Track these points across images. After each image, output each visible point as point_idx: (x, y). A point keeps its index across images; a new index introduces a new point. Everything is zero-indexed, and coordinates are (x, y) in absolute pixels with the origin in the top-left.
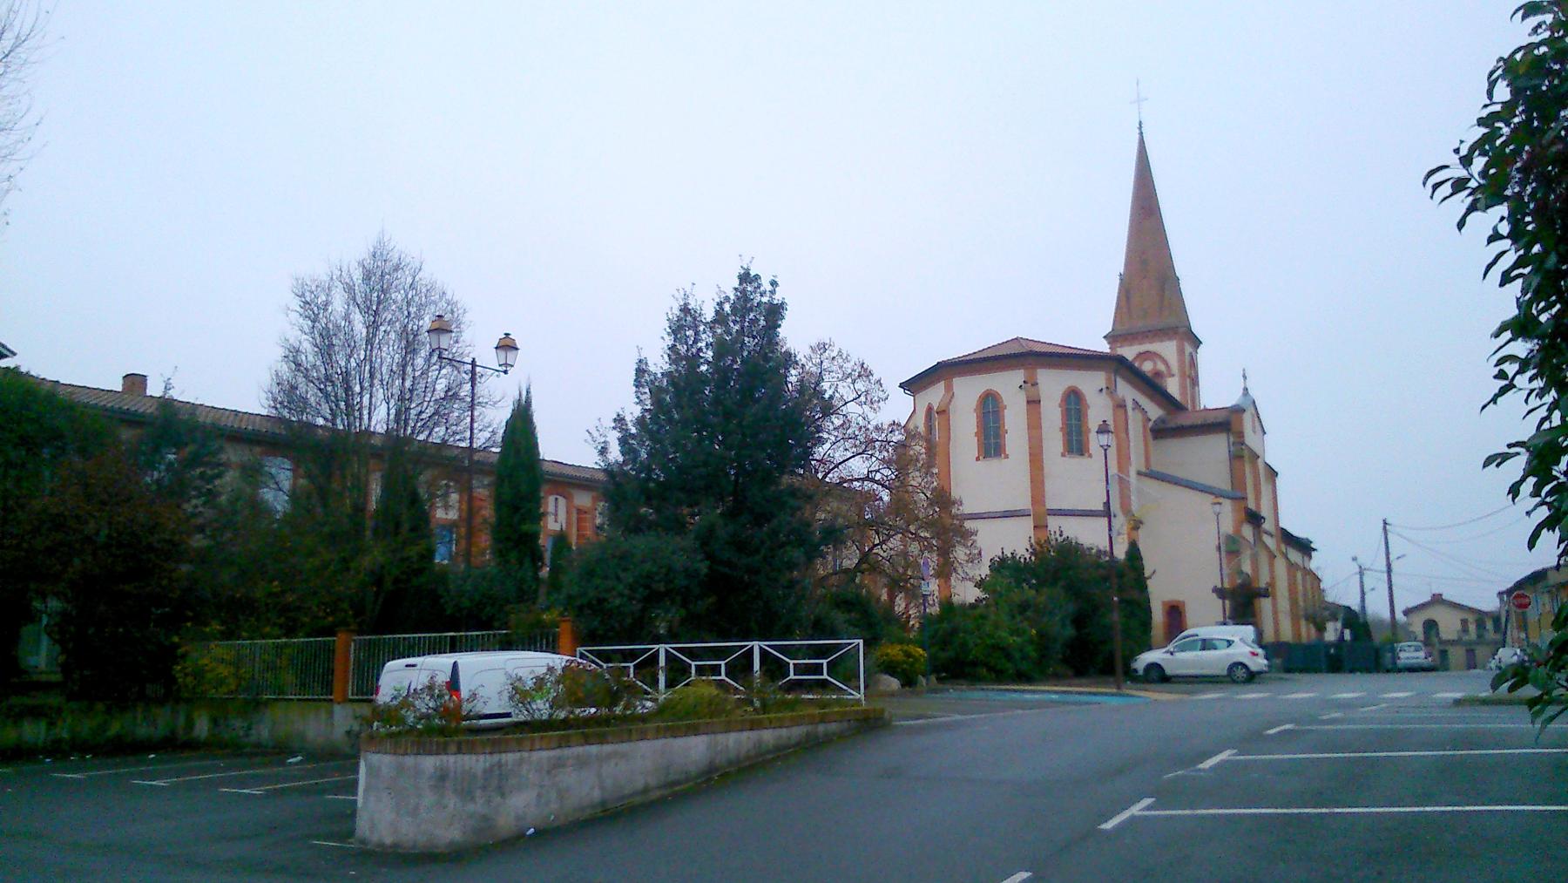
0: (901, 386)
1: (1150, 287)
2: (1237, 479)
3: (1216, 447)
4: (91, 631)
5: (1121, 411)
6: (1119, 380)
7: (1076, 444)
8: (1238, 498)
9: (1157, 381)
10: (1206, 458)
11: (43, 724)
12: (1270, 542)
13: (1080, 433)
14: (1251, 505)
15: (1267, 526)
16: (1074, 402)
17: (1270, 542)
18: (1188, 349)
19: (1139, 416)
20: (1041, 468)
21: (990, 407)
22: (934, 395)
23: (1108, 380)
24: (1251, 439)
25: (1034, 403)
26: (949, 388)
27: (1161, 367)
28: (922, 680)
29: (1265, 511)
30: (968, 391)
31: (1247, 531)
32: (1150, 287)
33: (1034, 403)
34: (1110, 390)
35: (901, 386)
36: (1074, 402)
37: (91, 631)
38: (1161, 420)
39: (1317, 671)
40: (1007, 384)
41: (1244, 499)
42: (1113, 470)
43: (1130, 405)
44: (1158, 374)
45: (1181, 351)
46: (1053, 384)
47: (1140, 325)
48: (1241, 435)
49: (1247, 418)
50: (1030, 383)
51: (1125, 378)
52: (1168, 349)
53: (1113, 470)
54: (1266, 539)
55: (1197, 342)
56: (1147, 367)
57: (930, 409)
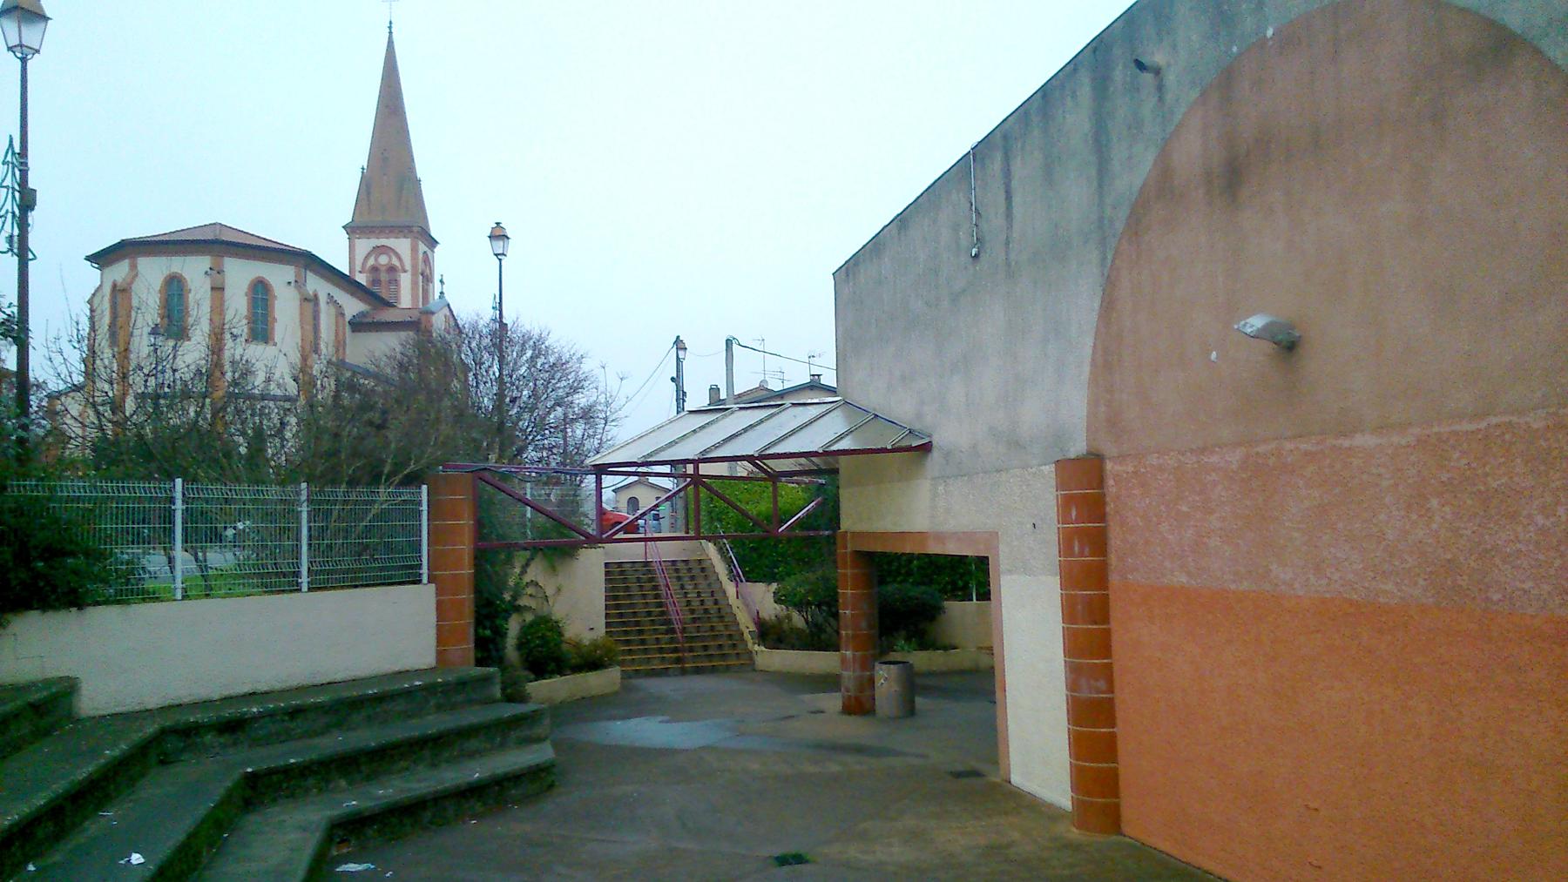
0: (88, 258)
1: (390, 195)
4: (1214, 355)
5: (309, 307)
6: (310, 275)
13: (265, 322)
16: (260, 293)
18: (422, 247)
19: (333, 310)
22: (120, 271)
25: (218, 289)
26: (133, 267)
27: (395, 262)
30: (153, 271)
32: (390, 195)
33: (218, 289)
34: (299, 284)
35: (88, 258)
36: (260, 293)
37: (1214, 355)
38: (362, 315)
39: (993, 718)
40: (194, 270)
43: (323, 299)
45: (414, 250)
46: (239, 274)
47: (377, 219)
52: (402, 245)
55: (433, 243)
57: (114, 286)
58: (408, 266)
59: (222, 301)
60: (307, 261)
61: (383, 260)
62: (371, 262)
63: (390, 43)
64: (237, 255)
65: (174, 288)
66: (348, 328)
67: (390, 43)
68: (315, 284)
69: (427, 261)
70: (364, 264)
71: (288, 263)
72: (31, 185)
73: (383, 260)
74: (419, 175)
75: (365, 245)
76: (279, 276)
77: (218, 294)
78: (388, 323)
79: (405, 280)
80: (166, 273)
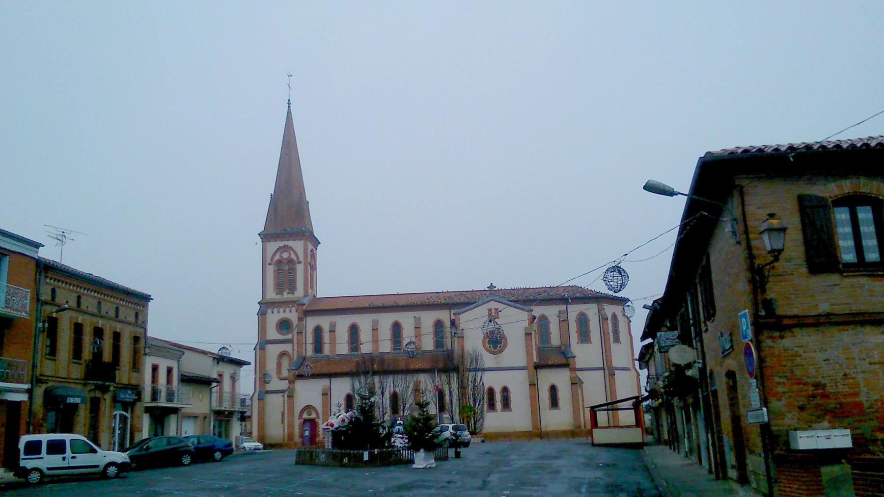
18: (310, 247)
27: (293, 256)
40: (551, 312)
45: (306, 250)
46: (574, 310)
52: (298, 246)
55: (316, 243)
58: (301, 259)
59: (293, 403)
61: (285, 255)
62: (277, 257)
63: (289, 112)
67: (289, 112)
69: (313, 256)
70: (272, 259)
73: (285, 255)
75: (273, 246)
78: (325, 310)
79: (300, 269)
80: (795, 197)
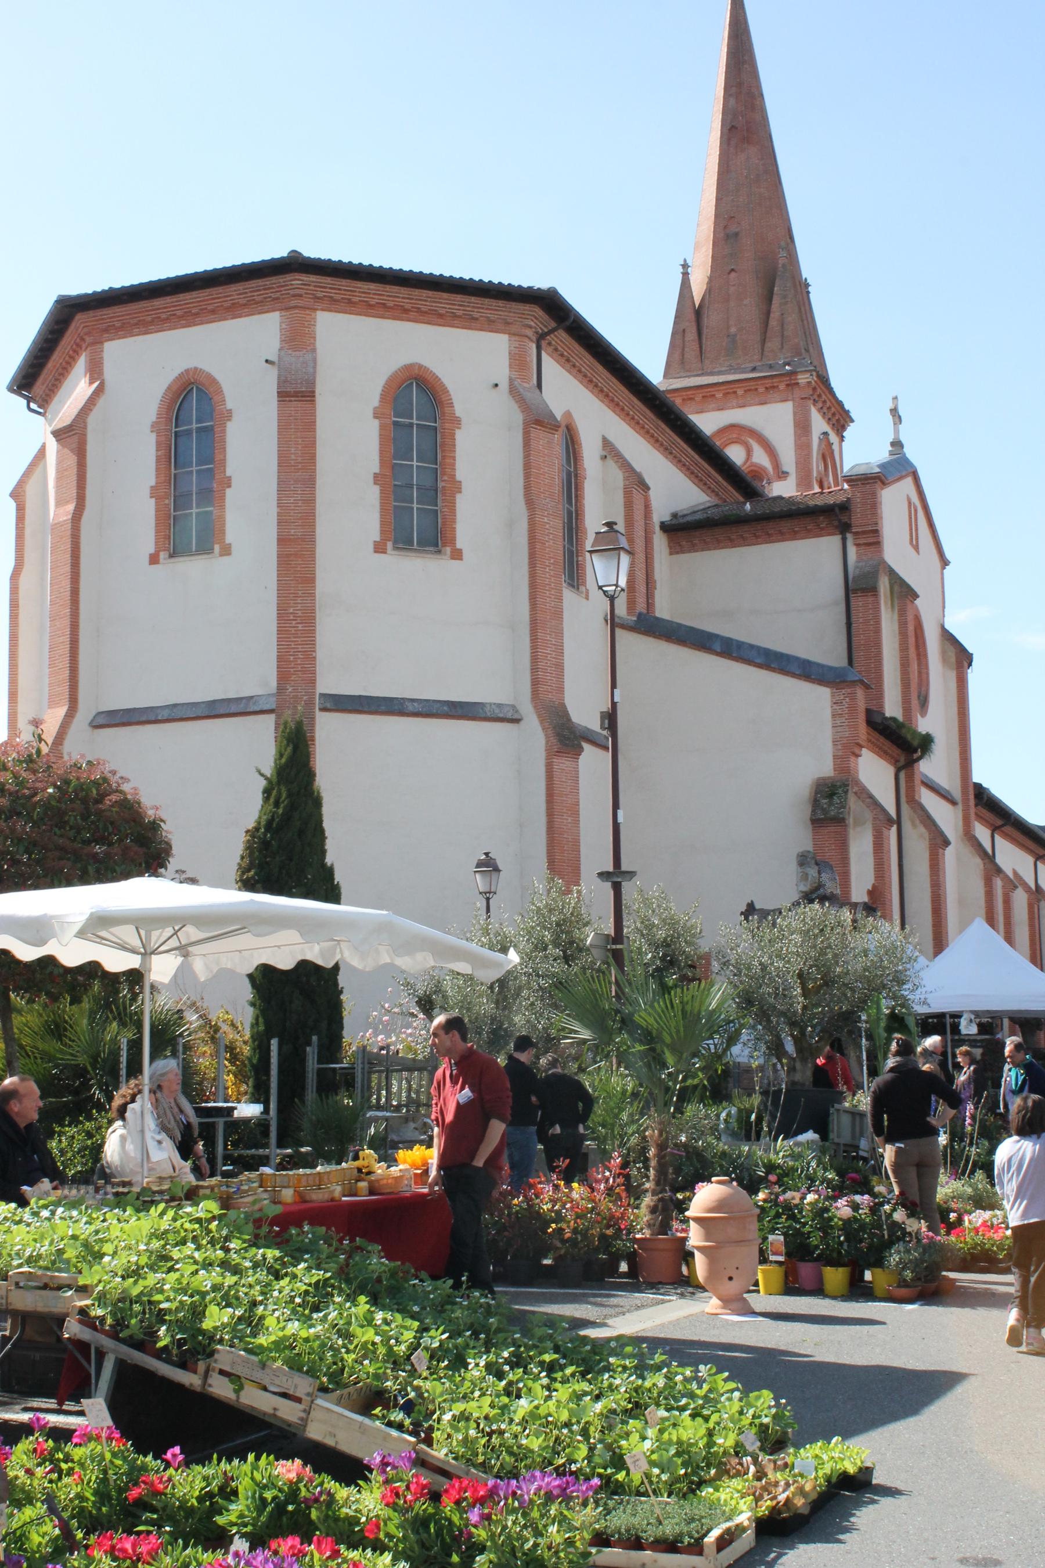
2: (858, 638)
3: (813, 564)
7: (419, 515)
8: (849, 676)
9: (756, 484)
10: (789, 585)
11: (513, 1460)
12: (947, 817)
14: (892, 708)
15: (936, 767)
16: (417, 412)
17: (947, 817)
18: (819, 424)
19: (618, 477)
20: (309, 580)
21: (191, 417)
23: (517, 361)
24: (896, 551)
25: (297, 395)
27: (761, 458)
28: (39, 1504)
29: (932, 722)
31: (875, 773)
33: (297, 395)
36: (417, 412)
40: (238, 351)
41: (873, 686)
42: (1036, 921)
44: (758, 473)
45: (802, 427)
46: (359, 354)
48: (872, 539)
49: (893, 502)
50: (298, 339)
51: (566, 361)
52: (774, 419)
53: (1036, 921)
54: (927, 799)
56: (735, 454)
59: (310, 426)
60: (550, 318)
64: (350, 306)
65: (191, 417)
66: (660, 541)
68: (565, 391)
71: (490, 325)
72: (12, 505)
74: (807, 271)
76: (472, 363)
77: (295, 407)
